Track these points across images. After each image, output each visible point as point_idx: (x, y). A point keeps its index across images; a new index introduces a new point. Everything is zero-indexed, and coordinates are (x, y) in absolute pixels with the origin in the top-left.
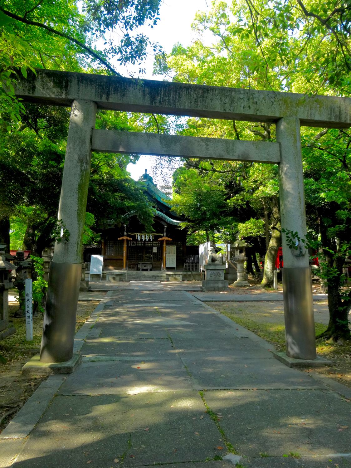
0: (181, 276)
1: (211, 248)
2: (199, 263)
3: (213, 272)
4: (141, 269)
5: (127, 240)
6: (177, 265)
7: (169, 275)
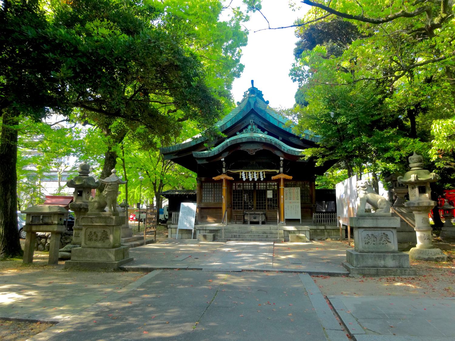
0: (308, 233)
1: (354, 189)
2: (336, 212)
3: (370, 233)
4: (249, 222)
5: (227, 180)
6: (302, 216)
7: (289, 232)
